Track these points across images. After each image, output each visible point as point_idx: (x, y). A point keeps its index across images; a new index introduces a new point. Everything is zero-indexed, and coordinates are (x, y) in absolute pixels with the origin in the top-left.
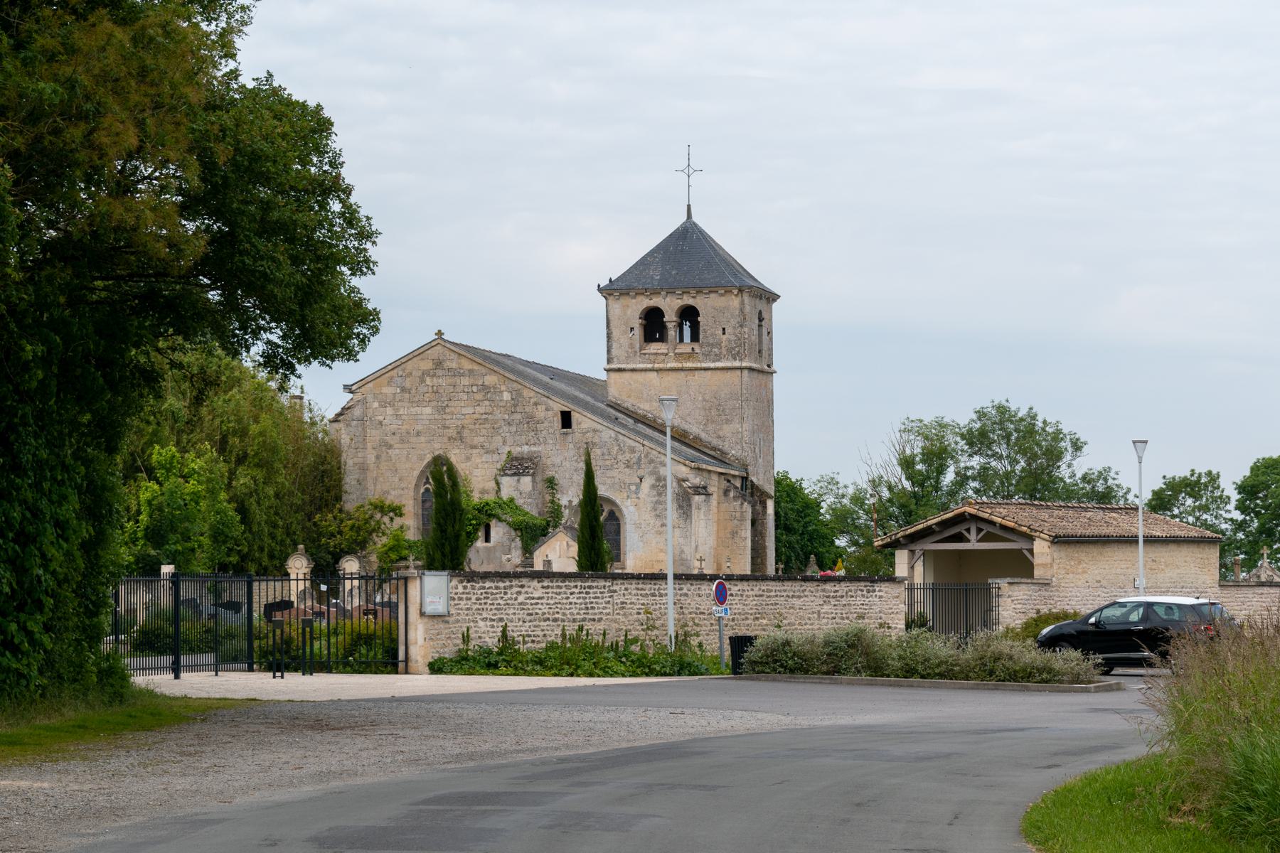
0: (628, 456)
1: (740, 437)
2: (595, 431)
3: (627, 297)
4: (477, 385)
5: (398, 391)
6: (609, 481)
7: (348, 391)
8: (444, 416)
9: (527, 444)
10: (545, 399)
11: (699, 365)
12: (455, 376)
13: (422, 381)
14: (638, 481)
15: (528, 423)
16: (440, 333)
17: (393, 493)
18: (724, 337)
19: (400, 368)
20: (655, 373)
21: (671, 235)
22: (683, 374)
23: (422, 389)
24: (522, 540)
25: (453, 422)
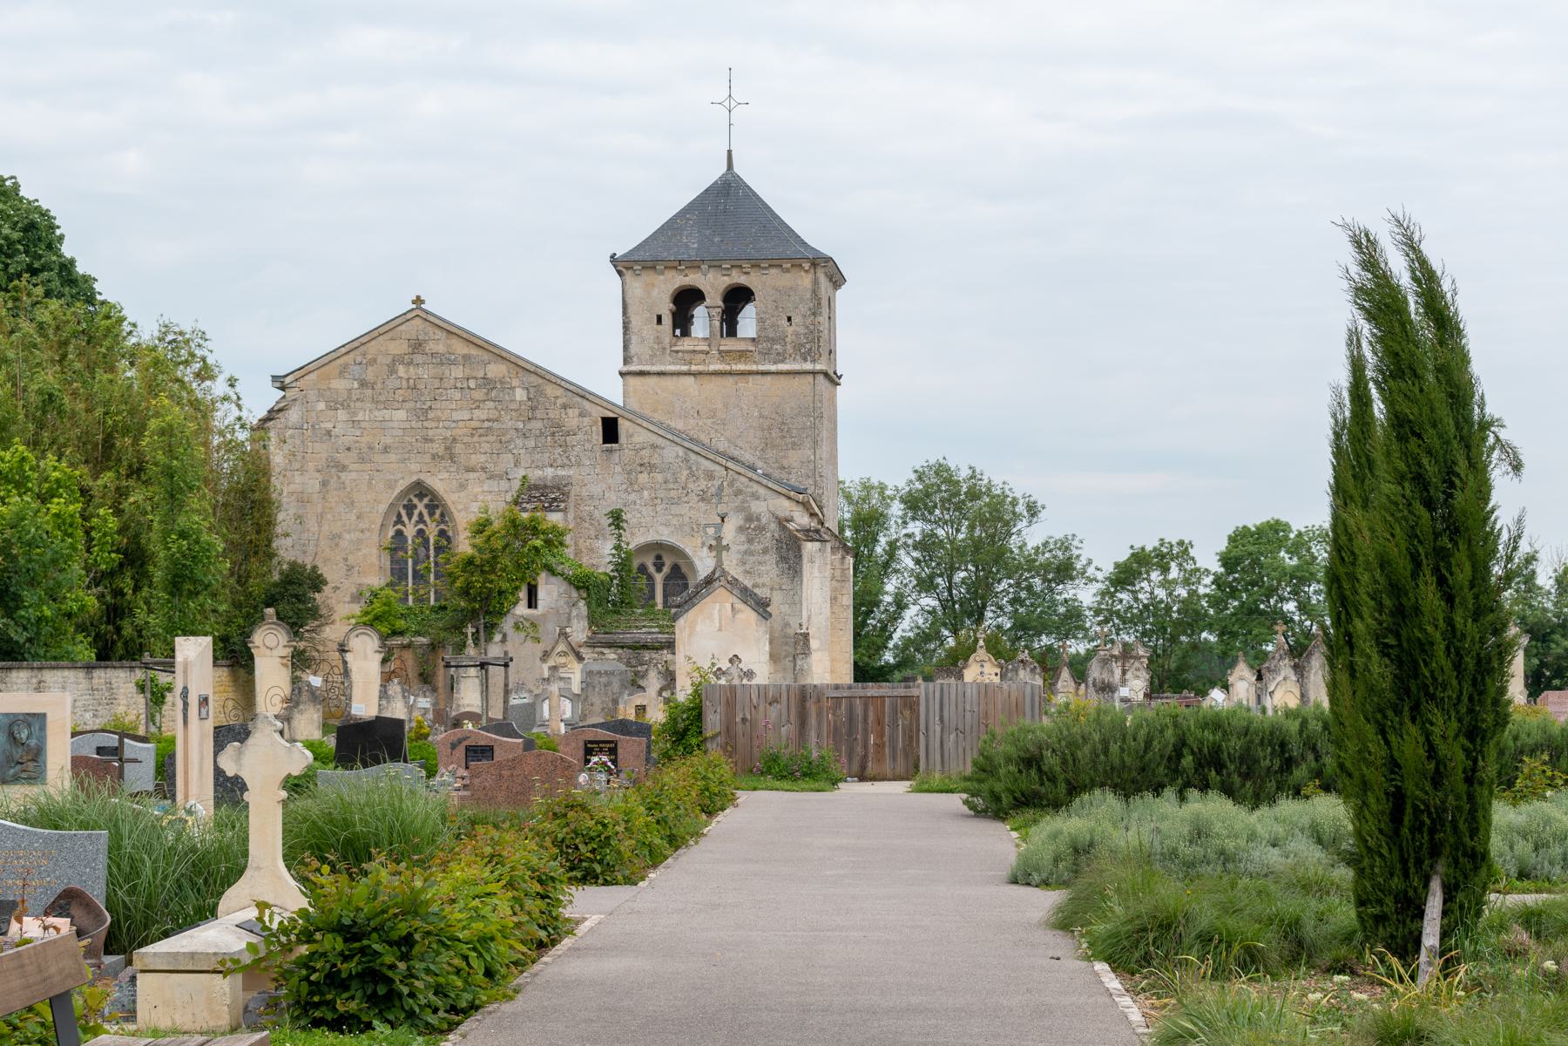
0: (703, 484)
1: (812, 467)
2: (654, 447)
3: (651, 272)
4: (475, 378)
5: (356, 385)
6: (674, 521)
7: (278, 385)
8: (426, 424)
9: (551, 466)
10: (579, 399)
11: (754, 368)
12: (442, 364)
13: (392, 371)
14: (719, 521)
15: (553, 434)
16: (418, 301)
17: (347, 536)
18: (790, 329)
19: (357, 352)
20: (692, 379)
21: (706, 190)
22: (731, 379)
23: (392, 383)
24: (589, 605)
25: (438, 433)
